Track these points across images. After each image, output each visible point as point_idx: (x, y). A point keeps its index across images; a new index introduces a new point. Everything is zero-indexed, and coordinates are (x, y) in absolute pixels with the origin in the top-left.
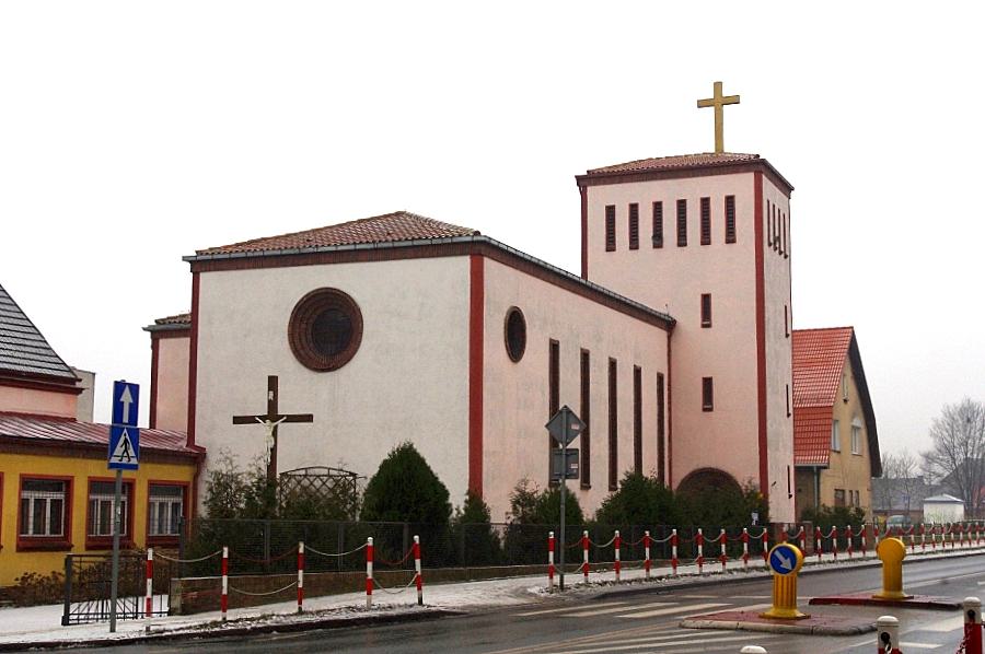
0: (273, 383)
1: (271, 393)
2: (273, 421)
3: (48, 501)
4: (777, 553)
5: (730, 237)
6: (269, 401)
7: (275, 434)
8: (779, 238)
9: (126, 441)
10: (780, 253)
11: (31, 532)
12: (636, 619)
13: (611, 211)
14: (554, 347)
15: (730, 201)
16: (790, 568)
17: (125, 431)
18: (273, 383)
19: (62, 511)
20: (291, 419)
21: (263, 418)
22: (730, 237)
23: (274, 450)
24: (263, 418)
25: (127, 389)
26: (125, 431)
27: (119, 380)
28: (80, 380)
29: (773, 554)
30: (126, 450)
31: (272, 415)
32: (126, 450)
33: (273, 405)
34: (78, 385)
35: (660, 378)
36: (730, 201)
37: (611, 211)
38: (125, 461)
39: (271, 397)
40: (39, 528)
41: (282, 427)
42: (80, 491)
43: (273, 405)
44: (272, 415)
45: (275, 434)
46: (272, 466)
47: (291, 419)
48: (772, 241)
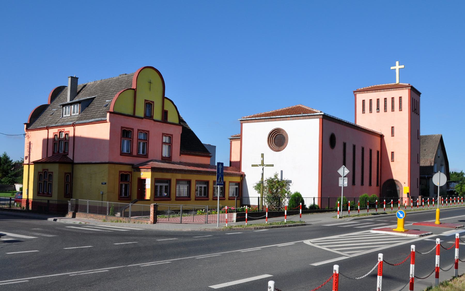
0: (263, 155)
1: (262, 158)
2: (262, 166)
3: (203, 187)
4: (399, 213)
5: (400, 109)
6: (262, 160)
7: (263, 169)
8: (416, 109)
9: (220, 178)
10: (416, 114)
11: (199, 195)
12: (381, 220)
13: (364, 101)
14: (345, 144)
15: (400, 98)
16: (402, 217)
17: (220, 175)
18: (263, 155)
19: (206, 189)
20: (267, 166)
21: (260, 165)
22: (400, 109)
23: (263, 174)
24: (260, 165)
25: (220, 164)
26: (220, 175)
27: (219, 162)
28: (211, 154)
29: (398, 212)
30: (220, 180)
31: (263, 164)
32: (220, 180)
33: (263, 161)
34: (210, 155)
35: (378, 152)
36: (400, 98)
37: (364, 101)
38: (220, 183)
39: (262, 159)
40: (201, 194)
41: (265, 168)
42: (211, 184)
43: (263, 161)
44: (263, 164)
45: (263, 169)
46: (262, 178)
47: (267, 166)
48: (414, 110)
